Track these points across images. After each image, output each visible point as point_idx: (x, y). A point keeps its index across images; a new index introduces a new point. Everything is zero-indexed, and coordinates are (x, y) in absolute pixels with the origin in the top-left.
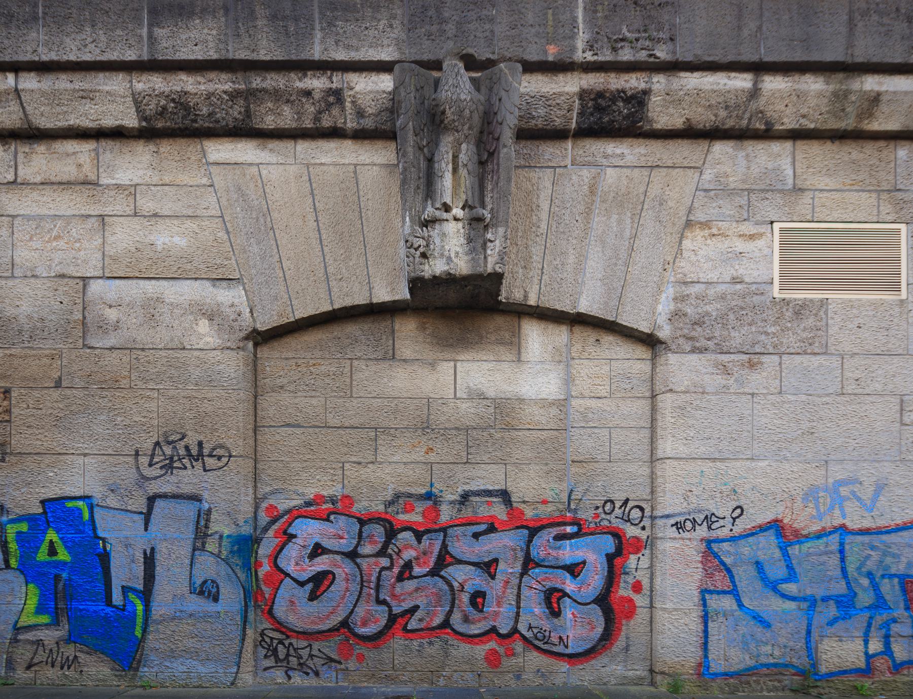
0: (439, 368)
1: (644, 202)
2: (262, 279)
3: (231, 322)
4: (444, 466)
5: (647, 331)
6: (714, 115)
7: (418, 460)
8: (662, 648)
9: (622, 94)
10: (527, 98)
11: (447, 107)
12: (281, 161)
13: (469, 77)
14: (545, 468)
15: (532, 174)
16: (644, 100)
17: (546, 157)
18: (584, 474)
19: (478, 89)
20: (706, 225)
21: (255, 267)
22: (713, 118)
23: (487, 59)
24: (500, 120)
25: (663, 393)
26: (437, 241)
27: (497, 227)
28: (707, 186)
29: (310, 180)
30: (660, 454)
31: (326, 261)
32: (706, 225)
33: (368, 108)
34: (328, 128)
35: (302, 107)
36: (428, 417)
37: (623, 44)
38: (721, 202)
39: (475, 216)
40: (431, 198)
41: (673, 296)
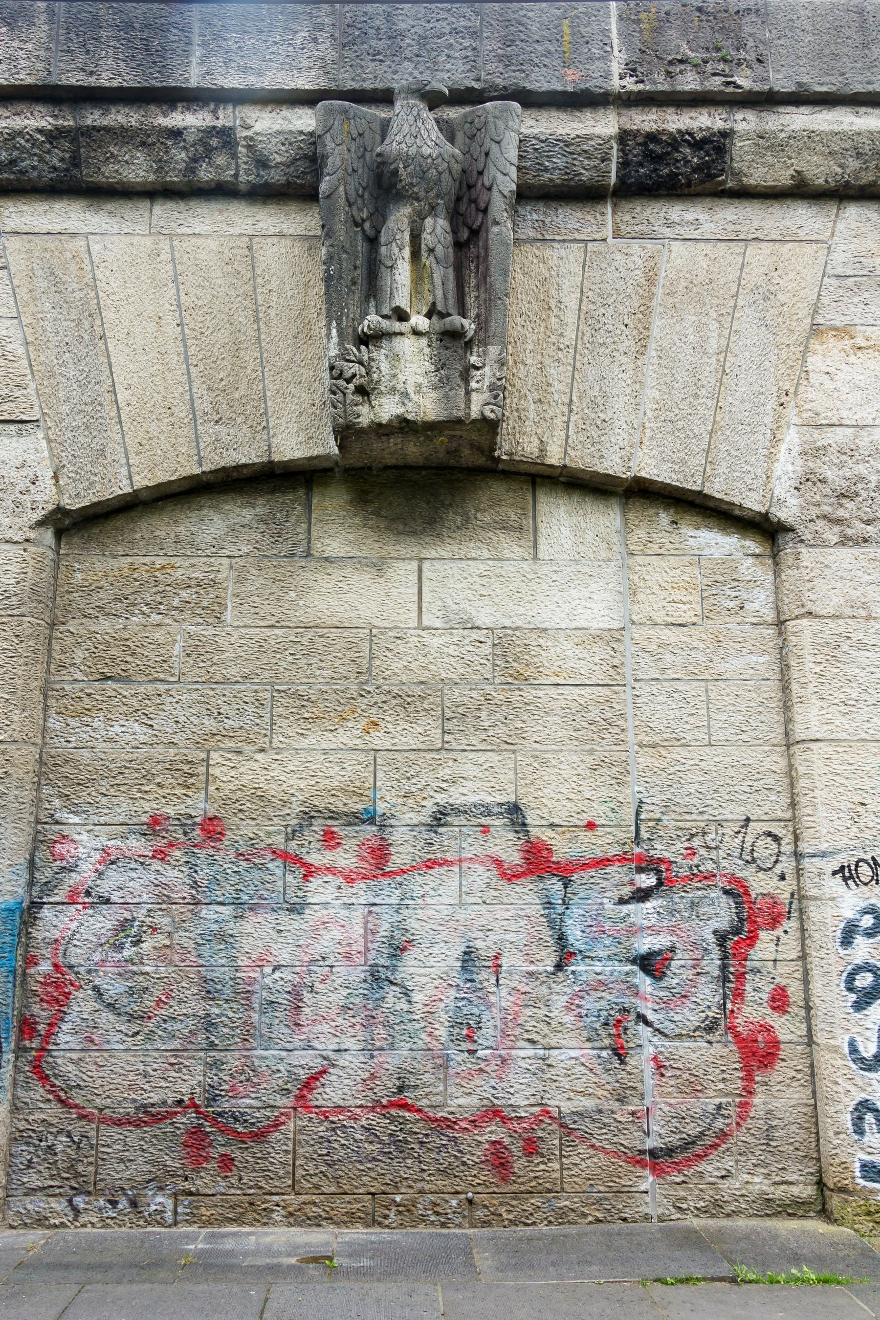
0: (390, 573)
1: (737, 295)
2: (79, 420)
3: (19, 495)
4: (398, 756)
5: (757, 508)
6: (840, 166)
7: (351, 744)
8: (838, 1133)
9: (687, 137)
11: (401, 166)
12: (126, 231)
13: (437, 121)
14: (589, 759)
15: (548, 252)
16: (724, 145)
17: (569, 226)
18: (663, 770)
19: (451, 139)
20: (843, 332)
21: (67, 400)
22: (839, 170)
23: (467, 88)
24: (487, 184)
25: (797, 617)
26: (385, 366)
28: (839, 271)
29: (173, 260)
30: (799, 733)
31: (194, 390)
32: (843, 332)
33: (276, 156)
34: (207, 182)
35: (166, 152)
36: (370, 662)
37: (682, 67)
38: (867, 295)
39: (448, 327)
40: (375, 297)
41: (798, 449)
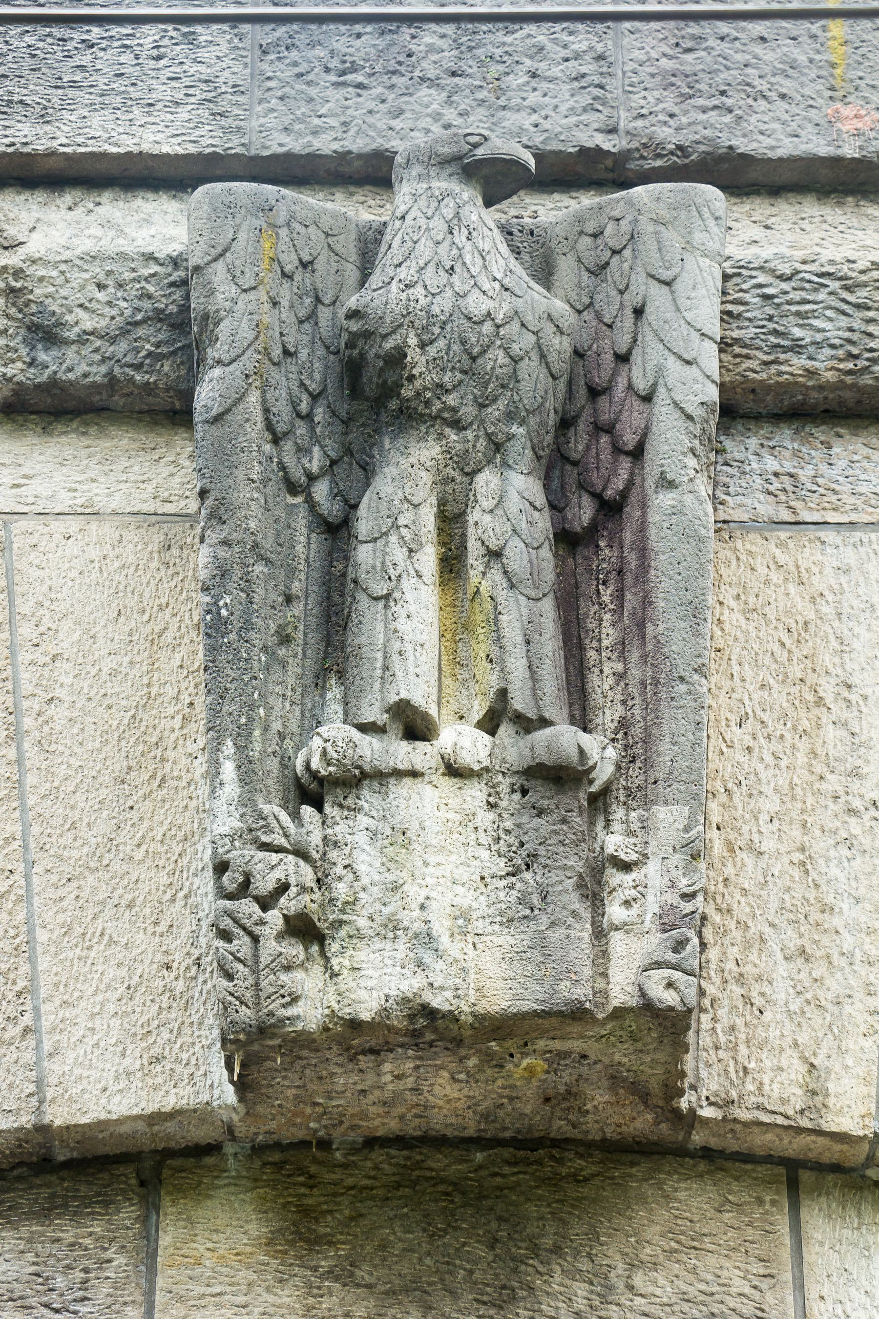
10: (762, 279)
11: (413, 341)
23: (584, 151)
24: (641, 385)
27: (647, 803)
33: (80, 313)
39: (542, 755)
40: (341, 674)
